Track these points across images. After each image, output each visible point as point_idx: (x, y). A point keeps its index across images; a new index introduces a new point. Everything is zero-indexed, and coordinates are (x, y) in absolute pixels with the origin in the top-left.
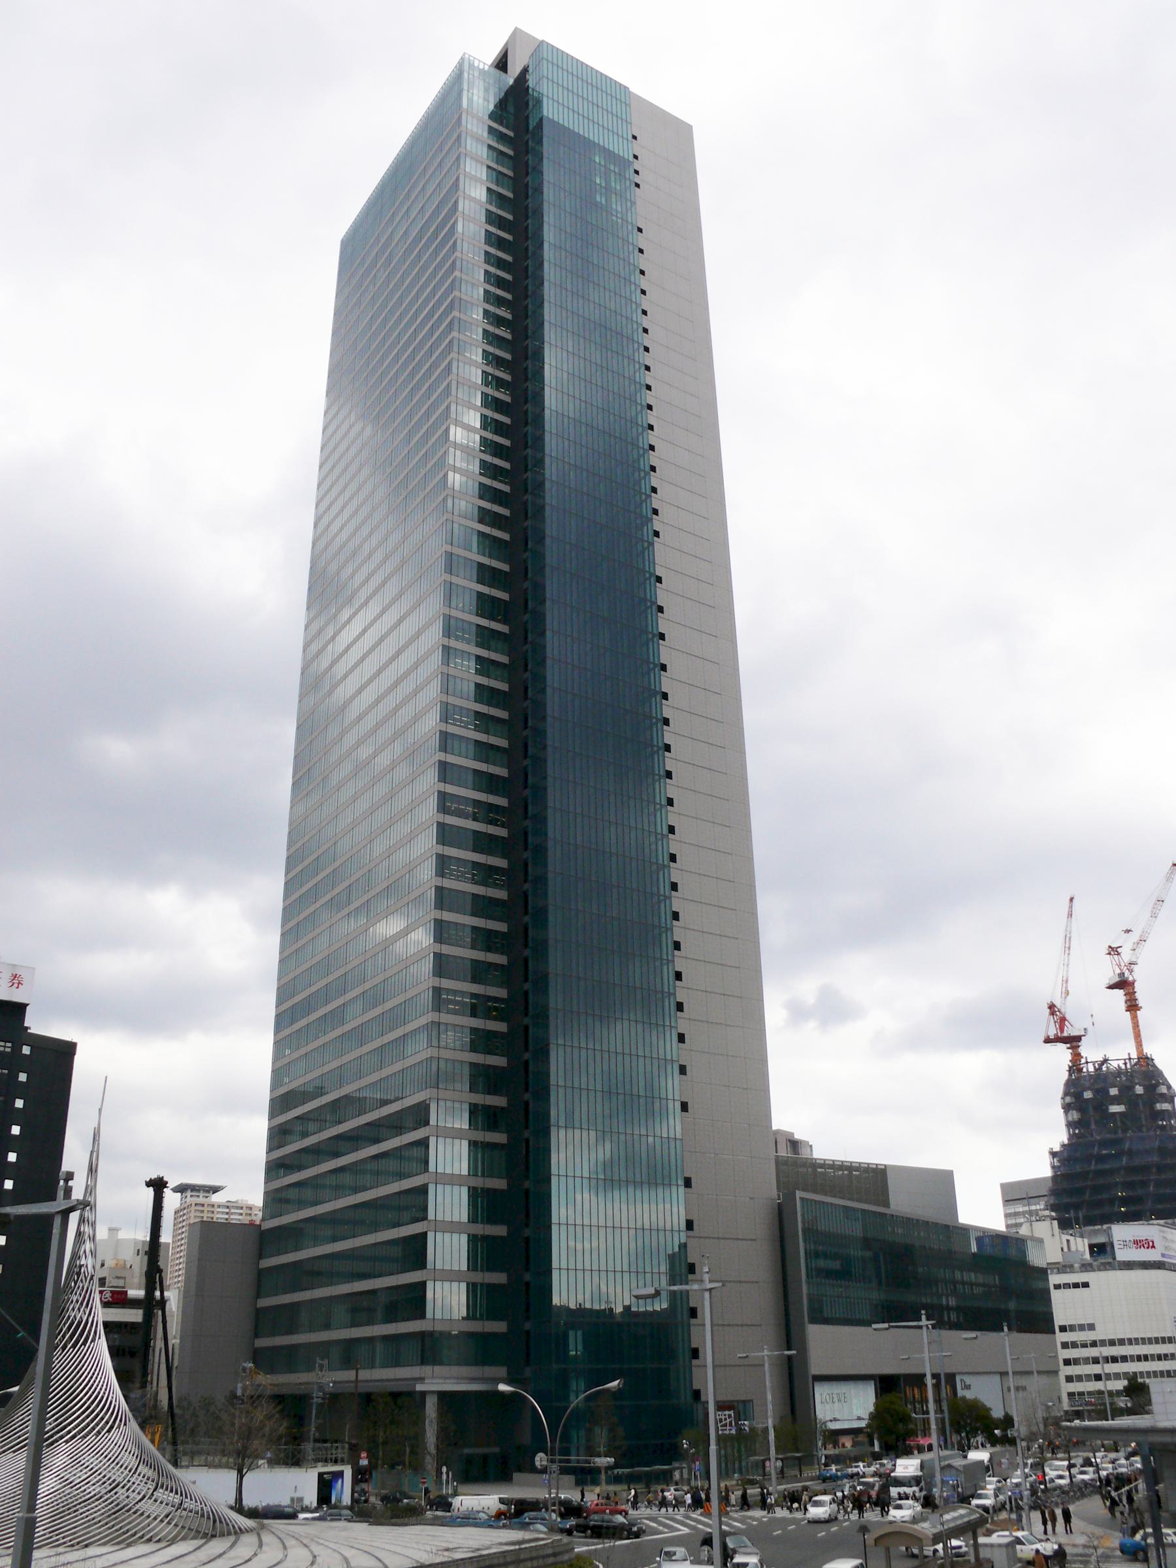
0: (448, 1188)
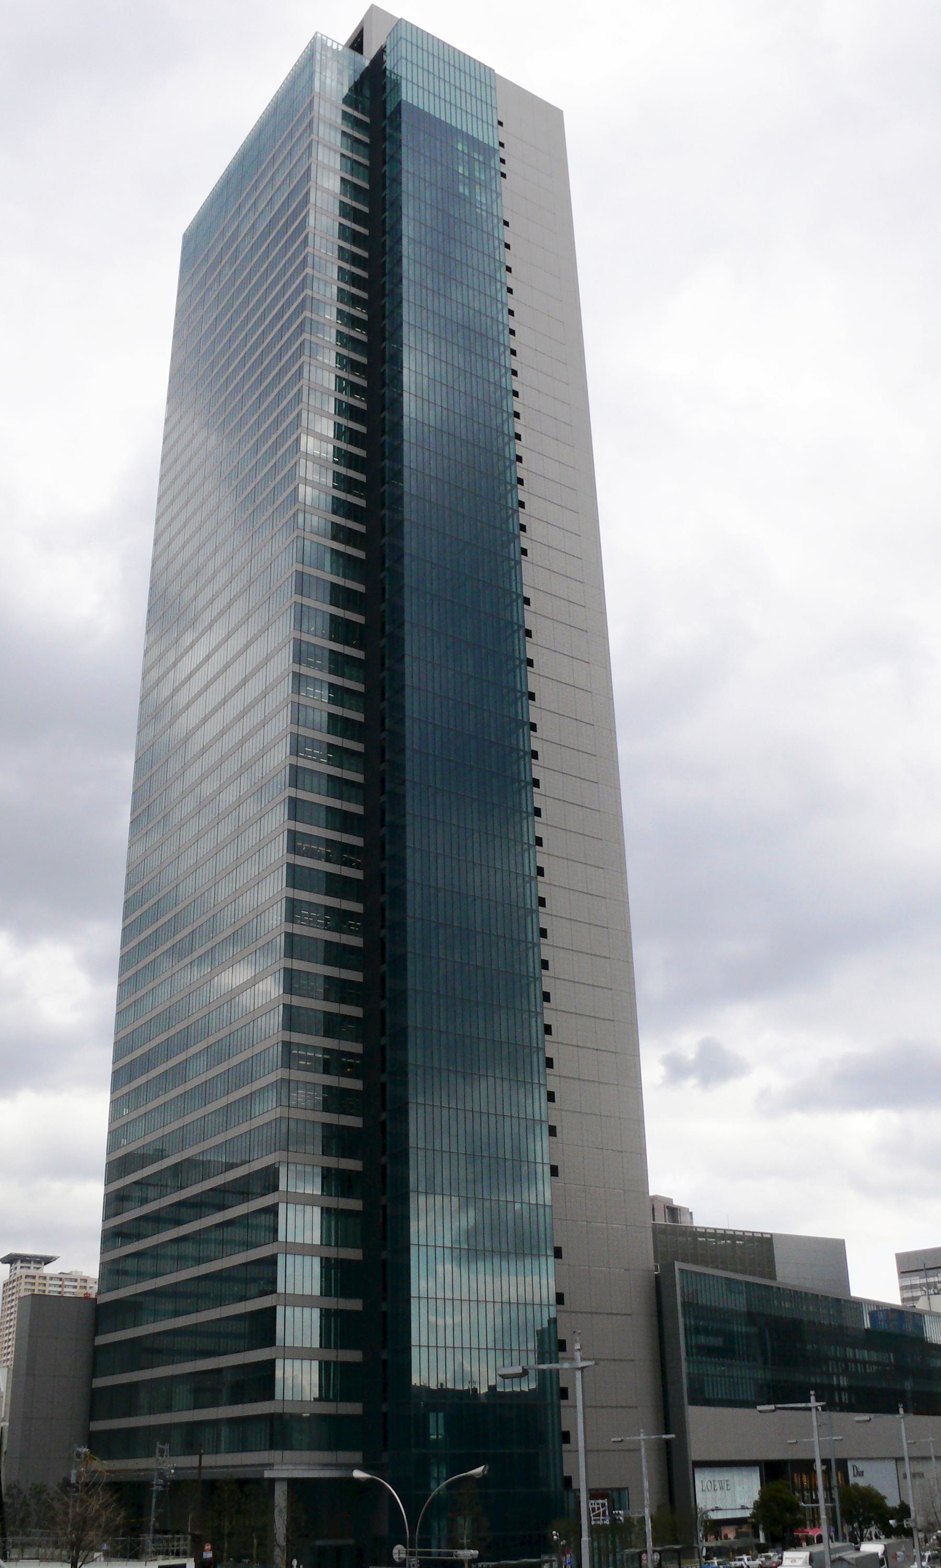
0: (299, 1258)
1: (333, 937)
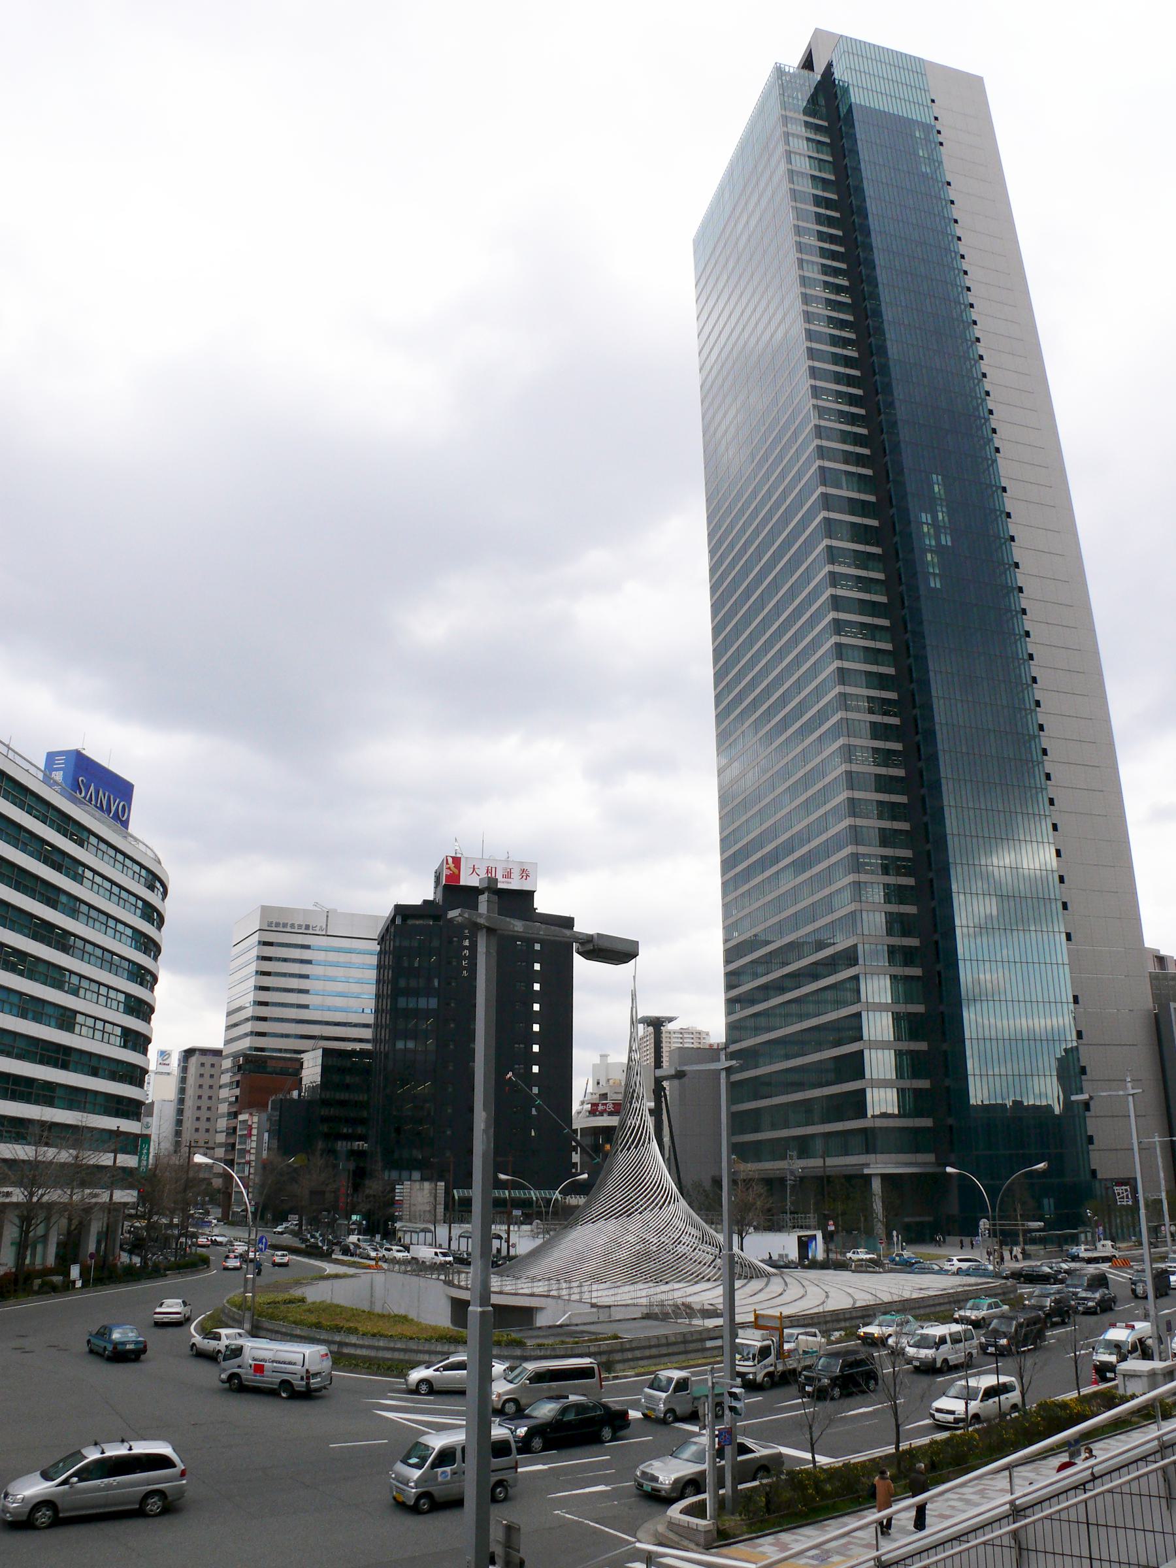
0: (877, 1014)
1: (882, 771)
